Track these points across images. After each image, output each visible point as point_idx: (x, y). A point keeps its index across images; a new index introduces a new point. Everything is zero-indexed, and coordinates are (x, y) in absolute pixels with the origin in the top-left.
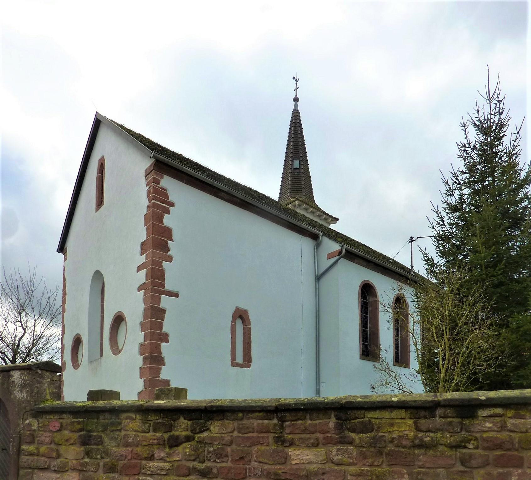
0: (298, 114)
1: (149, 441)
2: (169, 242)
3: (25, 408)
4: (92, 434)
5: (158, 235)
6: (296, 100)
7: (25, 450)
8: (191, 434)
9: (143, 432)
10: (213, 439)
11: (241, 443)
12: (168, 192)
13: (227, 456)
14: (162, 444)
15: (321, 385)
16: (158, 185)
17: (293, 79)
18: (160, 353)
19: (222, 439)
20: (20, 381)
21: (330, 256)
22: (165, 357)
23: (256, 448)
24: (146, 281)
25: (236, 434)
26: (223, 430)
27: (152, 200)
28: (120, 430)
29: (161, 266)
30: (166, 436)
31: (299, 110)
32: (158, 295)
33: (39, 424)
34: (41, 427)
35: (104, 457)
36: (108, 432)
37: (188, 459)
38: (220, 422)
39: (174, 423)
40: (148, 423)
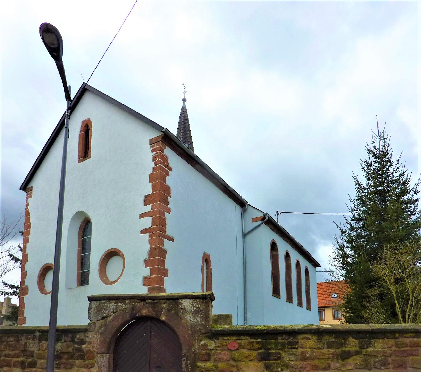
0: (186, 111)
1: (325, 356)
2: (169, 197)
3: (200, 331)
4: (270, 351)
5: (163, 192)
6: (184, 100)
7: (201, 367)
8: (359, 349)
9: (319, 349)
10: (378, 352)
11: (399, 355)
12: (168, 159)
13: (389, 364)
14: (335, 357)
15: (248, 314)
16: (163, 153)
17: (183, 85)
18: (163, 285)
19: (384, 352)
20: (192, 308)
21: (254, 220)
22: (166, 289)
23: (411, 358)
24: (152, 226)
25: (394, 348)
26: (385, 346)
27: (159, 164)
28: (297, 348)
29: (164, 216)
30: (338, 351)
31: (186, 108)
32: (163, 238)
33: (215, 344)
34: (218, 347)
35: (284, 369)
36: (286, 349)
37: (358, 368)
38: (381, 340)
39: (344, 342)
40: (323, 342)
